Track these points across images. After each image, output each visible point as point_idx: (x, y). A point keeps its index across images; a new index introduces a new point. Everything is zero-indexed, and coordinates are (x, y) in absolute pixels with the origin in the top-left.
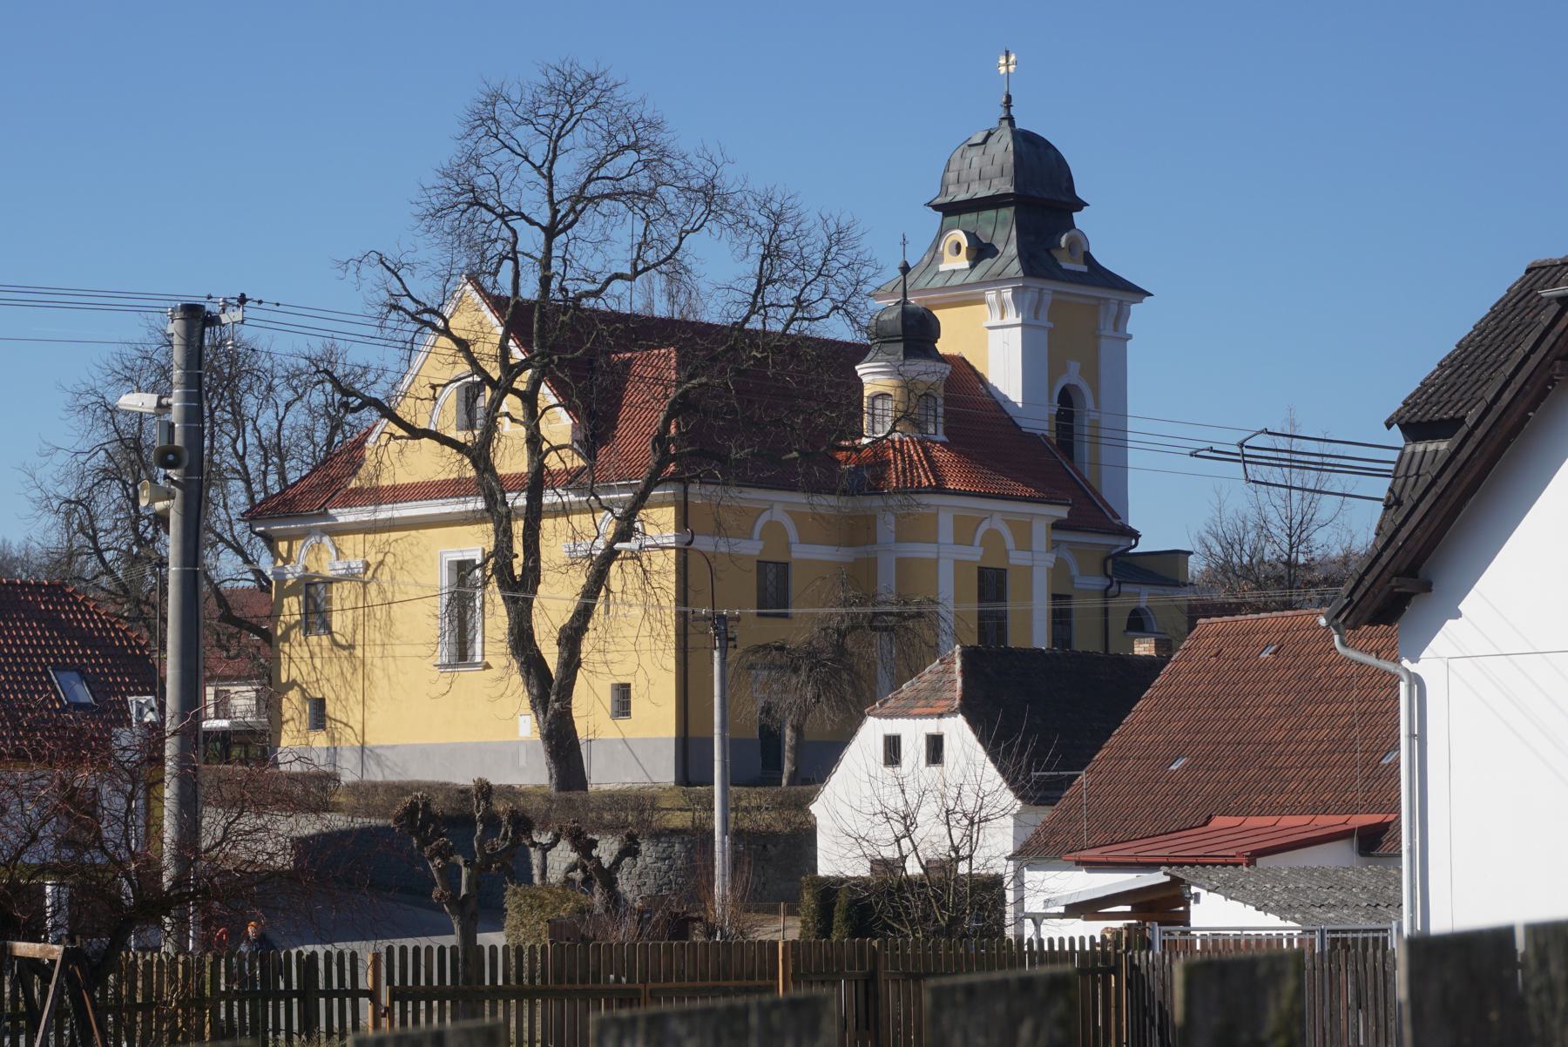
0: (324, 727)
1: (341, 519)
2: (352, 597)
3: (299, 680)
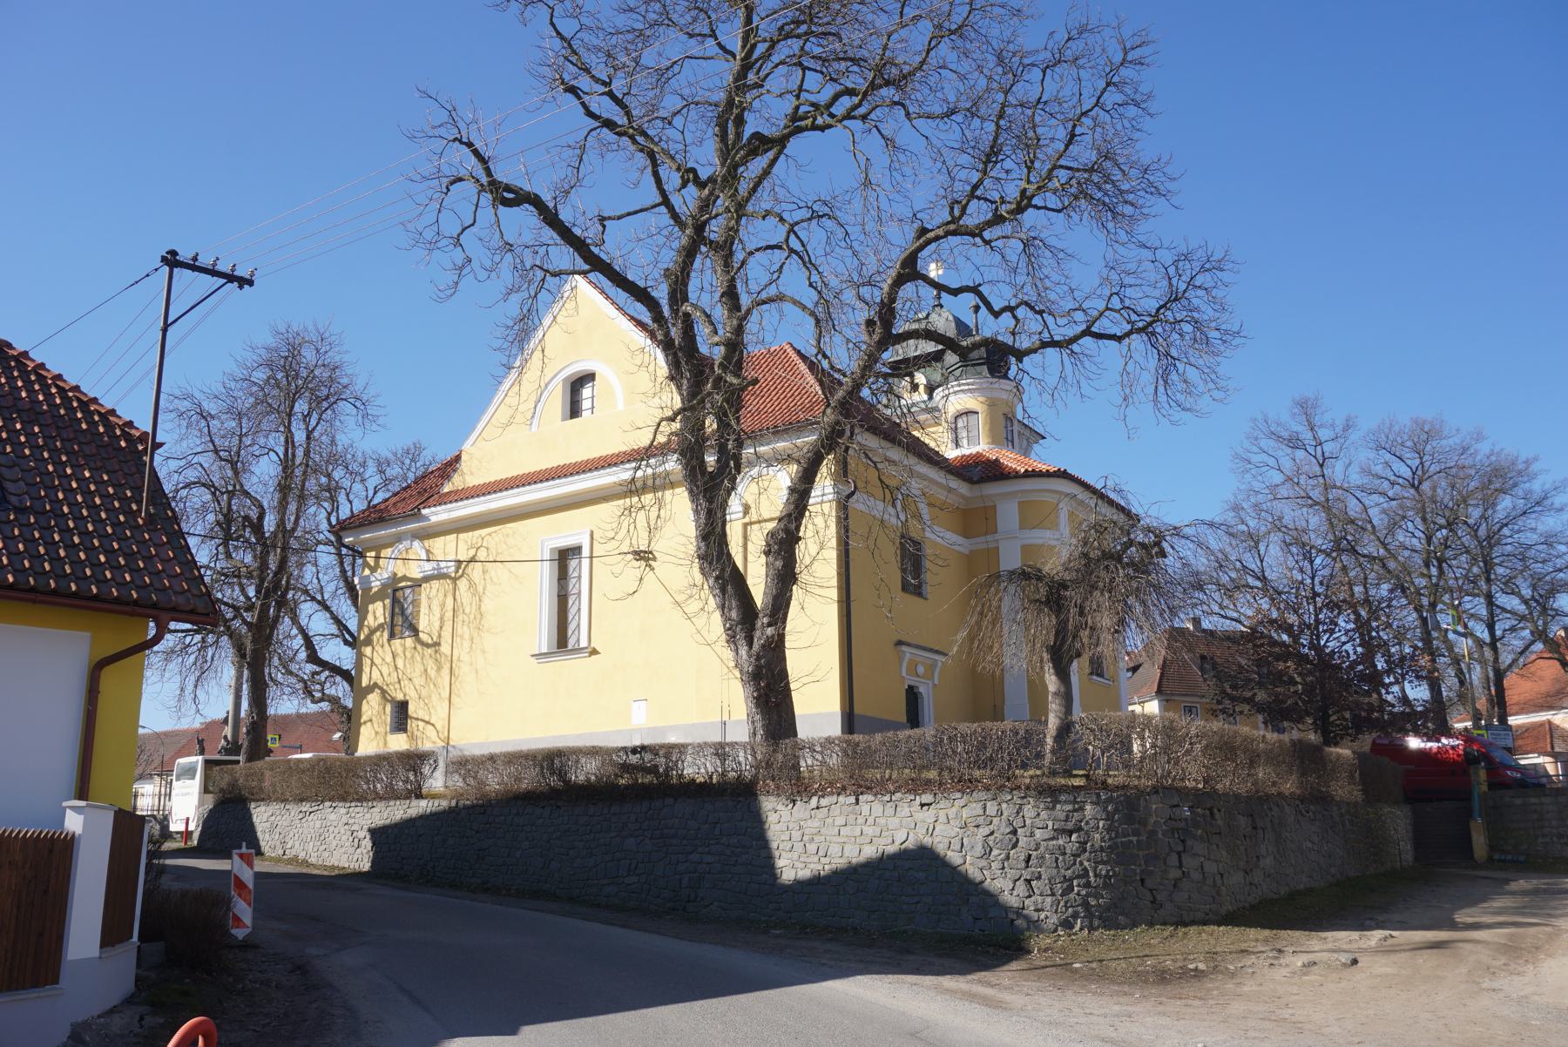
0: (405, 730)
1: (434, 519)
2: (441, 595)
3: (380, 682)
